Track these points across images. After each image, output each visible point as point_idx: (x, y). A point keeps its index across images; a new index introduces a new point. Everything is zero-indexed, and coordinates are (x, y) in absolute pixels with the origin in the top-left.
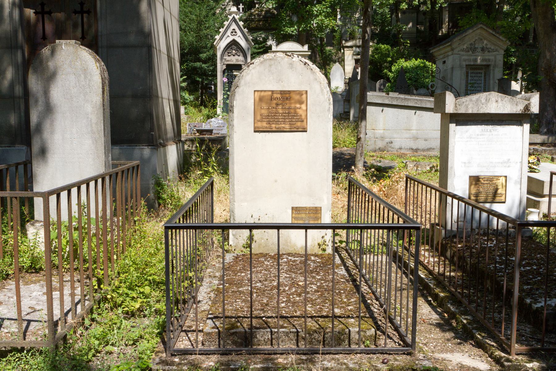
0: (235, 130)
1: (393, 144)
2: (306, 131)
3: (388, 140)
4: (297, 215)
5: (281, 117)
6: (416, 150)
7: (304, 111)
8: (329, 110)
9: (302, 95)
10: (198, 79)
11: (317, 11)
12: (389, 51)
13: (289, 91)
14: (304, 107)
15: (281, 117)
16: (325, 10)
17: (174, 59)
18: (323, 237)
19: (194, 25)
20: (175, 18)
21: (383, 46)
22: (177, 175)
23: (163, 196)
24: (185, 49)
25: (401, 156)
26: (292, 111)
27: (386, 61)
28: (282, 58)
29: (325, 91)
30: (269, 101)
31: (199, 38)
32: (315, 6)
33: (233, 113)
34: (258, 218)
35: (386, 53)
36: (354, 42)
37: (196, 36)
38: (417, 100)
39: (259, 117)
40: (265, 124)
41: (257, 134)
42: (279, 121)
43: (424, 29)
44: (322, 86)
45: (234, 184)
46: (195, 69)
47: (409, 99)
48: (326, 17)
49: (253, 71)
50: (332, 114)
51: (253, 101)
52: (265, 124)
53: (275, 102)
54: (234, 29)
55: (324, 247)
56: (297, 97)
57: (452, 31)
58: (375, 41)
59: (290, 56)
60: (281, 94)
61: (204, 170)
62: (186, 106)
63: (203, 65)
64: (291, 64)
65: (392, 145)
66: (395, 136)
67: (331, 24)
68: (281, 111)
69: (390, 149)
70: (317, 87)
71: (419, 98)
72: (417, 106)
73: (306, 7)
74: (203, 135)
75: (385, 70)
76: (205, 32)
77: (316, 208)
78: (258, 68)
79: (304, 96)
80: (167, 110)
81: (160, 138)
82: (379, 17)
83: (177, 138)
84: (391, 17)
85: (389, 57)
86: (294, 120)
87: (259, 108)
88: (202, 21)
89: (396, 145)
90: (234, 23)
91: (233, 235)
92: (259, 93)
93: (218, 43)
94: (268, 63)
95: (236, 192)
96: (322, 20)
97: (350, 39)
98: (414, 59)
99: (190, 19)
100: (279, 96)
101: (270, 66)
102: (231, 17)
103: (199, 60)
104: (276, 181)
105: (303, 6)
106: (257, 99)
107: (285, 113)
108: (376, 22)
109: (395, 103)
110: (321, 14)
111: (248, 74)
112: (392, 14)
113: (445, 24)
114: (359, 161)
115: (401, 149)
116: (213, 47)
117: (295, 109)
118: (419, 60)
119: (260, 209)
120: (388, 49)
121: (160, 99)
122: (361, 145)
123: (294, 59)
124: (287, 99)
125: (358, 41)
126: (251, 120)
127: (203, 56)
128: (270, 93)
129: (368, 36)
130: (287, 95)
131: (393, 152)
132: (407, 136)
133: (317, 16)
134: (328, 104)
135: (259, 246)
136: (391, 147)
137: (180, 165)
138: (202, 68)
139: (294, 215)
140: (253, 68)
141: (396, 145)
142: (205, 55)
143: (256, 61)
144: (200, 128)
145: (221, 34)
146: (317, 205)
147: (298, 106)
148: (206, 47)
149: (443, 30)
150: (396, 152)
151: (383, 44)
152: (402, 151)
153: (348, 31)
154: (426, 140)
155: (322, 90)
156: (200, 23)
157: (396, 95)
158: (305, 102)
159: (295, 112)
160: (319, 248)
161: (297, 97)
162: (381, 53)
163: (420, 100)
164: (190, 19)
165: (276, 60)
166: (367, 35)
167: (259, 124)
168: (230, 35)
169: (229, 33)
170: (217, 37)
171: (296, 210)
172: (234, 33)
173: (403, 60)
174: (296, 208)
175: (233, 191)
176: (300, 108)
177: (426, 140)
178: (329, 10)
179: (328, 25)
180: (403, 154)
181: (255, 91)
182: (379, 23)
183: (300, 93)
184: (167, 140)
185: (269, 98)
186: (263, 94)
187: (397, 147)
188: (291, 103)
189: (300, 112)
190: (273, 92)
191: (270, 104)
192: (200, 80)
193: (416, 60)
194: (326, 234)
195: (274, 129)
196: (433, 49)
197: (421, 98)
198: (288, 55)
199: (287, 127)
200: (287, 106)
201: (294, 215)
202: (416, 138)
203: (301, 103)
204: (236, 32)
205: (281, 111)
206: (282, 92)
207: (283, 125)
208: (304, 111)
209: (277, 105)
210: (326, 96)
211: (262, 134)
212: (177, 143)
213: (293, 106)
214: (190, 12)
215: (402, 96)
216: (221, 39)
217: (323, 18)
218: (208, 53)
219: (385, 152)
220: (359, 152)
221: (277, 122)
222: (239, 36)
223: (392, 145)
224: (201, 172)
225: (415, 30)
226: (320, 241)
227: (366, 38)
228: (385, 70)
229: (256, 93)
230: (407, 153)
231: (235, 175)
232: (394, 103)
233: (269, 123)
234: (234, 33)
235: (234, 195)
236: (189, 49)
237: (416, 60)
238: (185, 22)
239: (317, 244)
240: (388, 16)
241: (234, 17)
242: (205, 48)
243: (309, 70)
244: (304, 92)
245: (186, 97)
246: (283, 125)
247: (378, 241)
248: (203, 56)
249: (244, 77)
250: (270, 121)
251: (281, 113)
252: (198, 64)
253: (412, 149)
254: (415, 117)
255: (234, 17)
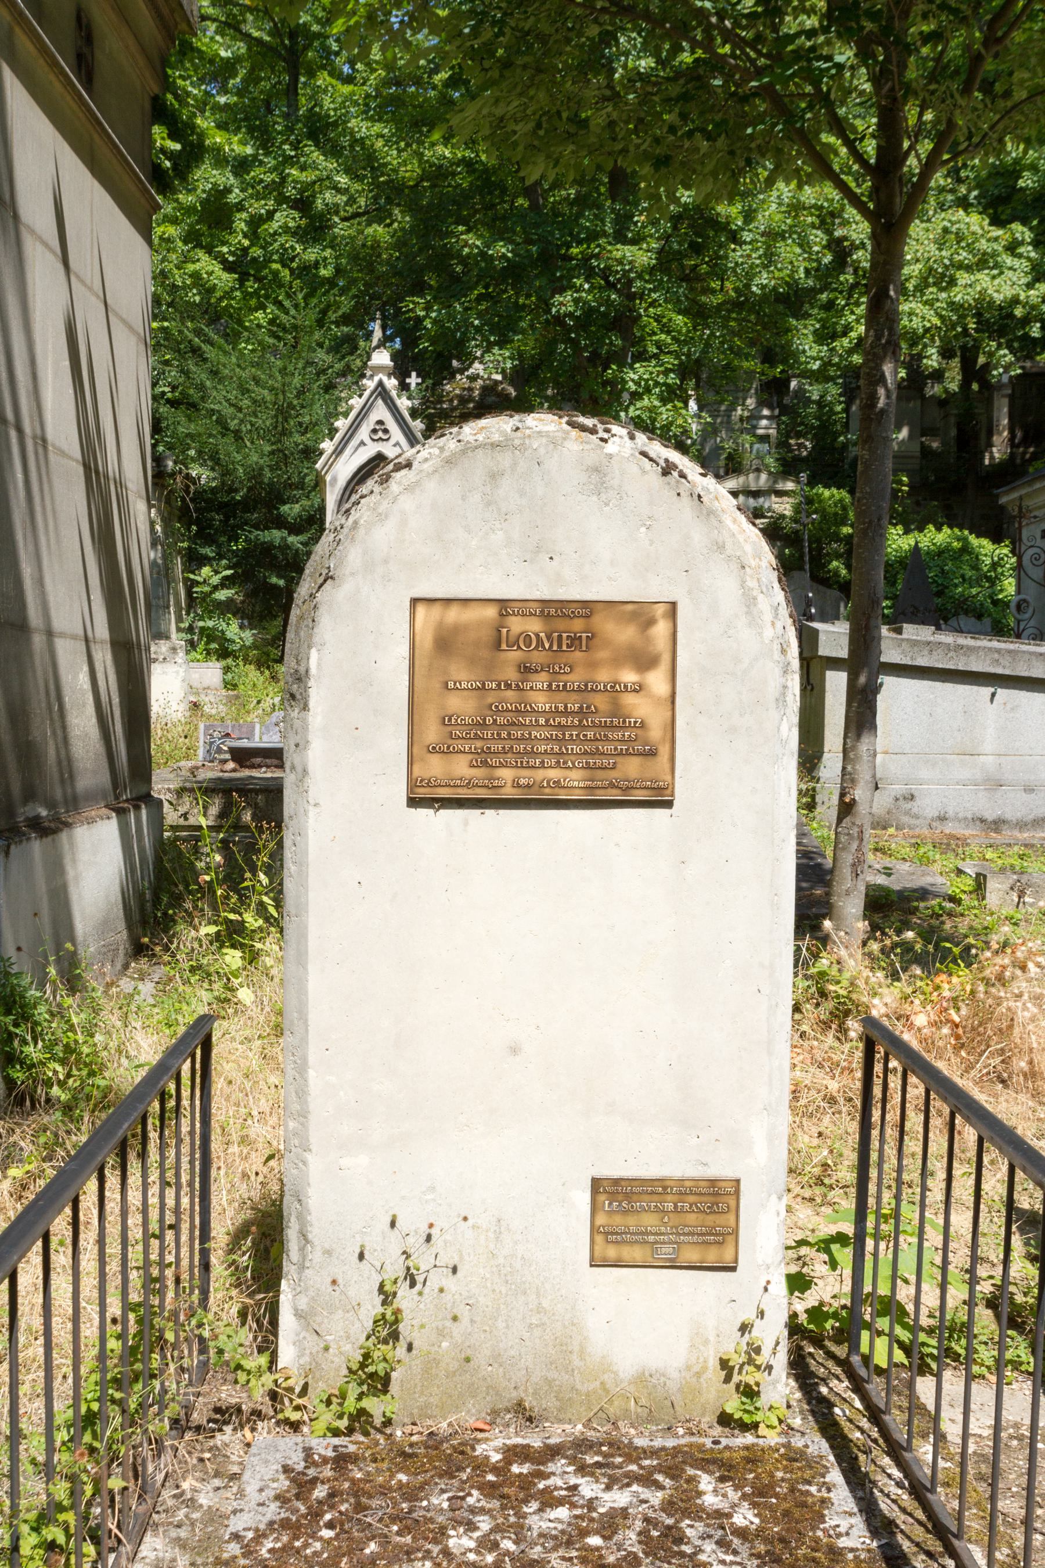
0: (312, 795)
1: (918, 802)
2: (668, 804)
3: (898, 789)
4: (618, 1219)
5: (545, 733)
6: (997, 825)
7: (657, 701)
8: (781, 700)
9: (651, 622)
10: (274, 580)
11: (637, 383)
12: (844, 508)
13: (585, 604)
14: (657, 681)
15: (545, 733)
16: (661, 379)
17: (120, 484)
18: (744, 1328)
19: (265, 420)
20: (130, 328)
21: (827, 493)
22: (121, 936)
23: (29, 1049)
24: (236, 491)
25: (949, 845)
26: (600, 702)
27: (837, 537)
28: (554, 443)
29: (764, 605)
30: (485, 653)
31: (281, 458)
32: (632, 368)
33: (305, 708)
34: (424, 1229)
35: (836, 514)
36: (742, 479)
37: (272, 453)
38: (998, 651)
39: (432, 733)
40: (461, 767)
41: (424, 814)
42: (533, 753)
43: (943, 444)
44: (751, 583)
45: (305, 1060)
46: (267, 549)
47: (971, 649)
48: (664, 401)
49: (407, 503)
50: (795, 720)
51: (404, 650)
52: (461, 767)
53: (514, 655)
54: (380, 422)
55: (750, 1377)
56: (625, 634)
57: (1024, 453)
58: (804, 476)
59: (593, 431)
60: (545, 616)
61: (227, 921)
62: (229, 661)
63: (292, 539)
64: (596, 470)
65: (914, 807)
66: (924, 773)
67: (680, 421)
68: (541, 701)
69: (905, 819)
70: (724, 585)
71: (1002, 645)
72: (999, 671)
73: (604, 371)
74: (253, 767)
75: (835, 563)
76: (298, 438)
77: (713, 1182)
78: (431, 486)
79: (661, 628)
80: (76, 682)
81: (30, 795)
82: (813, 409)
83: (130, 783)
84: (846, 410)
85: (845, 525)
86: (609, 747)
87: (438, 686)
88: (291, 406)
89: (928, 806)
90: (380, 402)
91: (298, 1314)
92: (436, 610)
93: (329, 465)
94: (482, 461)
95: (315, 1103)
96: (652, 409)
97: (727, 473)
98: (931, 527)
99: (255, 401)
100: (534, 626)
101: (494, 476)
102: (370, 384)
103: (280, 523)
104: (515, 1050)
105: (595, 366)
106: (426, 641)
107: (566, 713)
108: (802, 423)
109: (922, 661)
110: (648, 390)
111: (382, 517)
112: (848, 404)
113: (1000, 434)
114: (848, 893)
115: (942, 819)
116: (319, 483)
117: (615, 689)
118: (945, 528)
119: (432, 1189)
120: (841, 500)
121: (38, 641)
122: (854, 831)
123: (611, 448)
124: (575, 641)
125: (751, 476)
126: (395, 742)
127: (291, 510)
128: (491, 612)
129: (888, 396)
130: (578, 625)
131: (917, 831)
132: (965, 774)
133: (636, 396)
134: (778, 671)
135: (426, 1371)
136: (908, 813)
137: (140, 896)
138: (288, 547)
139: (601, 1219)
140: (409, 489)
141: (928, 806)
142: (297, 508)
143: (424, 454)
144: (245, 743)
145: (338, 436)
146: (720, 1169)
147: (629, 677)
148: (301, 485)
149: (994, 450)
150: (925, 831)
151: (827, 486)
152: (949, 828)
153: (723, 448)
154: (1029, 790)
155: (750, 602)
156: (284, 412)
157: (924, 633)
158: (666, 658)
159: (617, 710)
160: (727, 1380)
161: (625, 634)
162: (822, 512)
163: (1010, 652)
164: (255, 401)
165: (522, 448)
166: (881, 392)
167: (435, 767)
168: (367, 440)
169: (364, 433)
170: (327, 446)
171: (612, 1196)
172: (380, 434)
173: (900, 530)
174: (616, 1182)
175: (302, 1094)
176: (639, 689)
177: (1029, 790)
178: (672, 379)
179: (671, 423)
180: (951, 836)
181: (415, 601)
182: (813, 427)
183: (640, 614)
184: (74, 803)
185: (486, 635)
186: (453, 615)
187: (931, 812)
188: (593, 665)
189: (639, 707)
190: (503, 605)
191: (490, 666)
192: (281, 583)
193: (939, 529)
194: (761, 1314)
195: (509, 792)
196: (1007, 493)
197: (1012, 646)
198: (583, 428)
199: (574, 779)
200: (575, 678)
201: (601, 1219)
202: (995, 784)
203: (645, 662)
204: (386, 431)
205: (541, 701)
206: (551, 610)
207: (554, 774)
208: (657, 701)
209: (526, 669)
210: (769, 633)
211: (445, 814)
212: (120, 812)
213: (603, 676)
214: (257, 381)
215: (947, 638)
216: (338, 452)
217: (657, 403)
218: (305, 502)
219: (892, 830)
220: (847, 859)
221: (525, 758)
222: (397, 444)
223: (914, 807)
224: (212, 929)
225: (916, 448)
226: (732, 1346)
227: (881, 404)
228: (835, 563)
229: (421, 610)
230: (967, 832)
231: (312, 1017)
232: (922, 661)
233: (483, 759)
234: (380, 434)
235: (303, 1115)
236: (250, 489)
237: (939, 529)
238: (240, 410)
239: (713, 1363)
240: (839, 408)
241: (381, 384)
242: (297, 488)
243: (685, 499)
244: (660, 610)
245: (229, 635)
246: (554, 774)
247: (973, 1281)
248: (291, 510)
249: (361, 531)
250: (489, 752)
251: (545, 715)
252: (276, 535)
253: (982, 821)
254: (992, 712)
255: (381, 384)
